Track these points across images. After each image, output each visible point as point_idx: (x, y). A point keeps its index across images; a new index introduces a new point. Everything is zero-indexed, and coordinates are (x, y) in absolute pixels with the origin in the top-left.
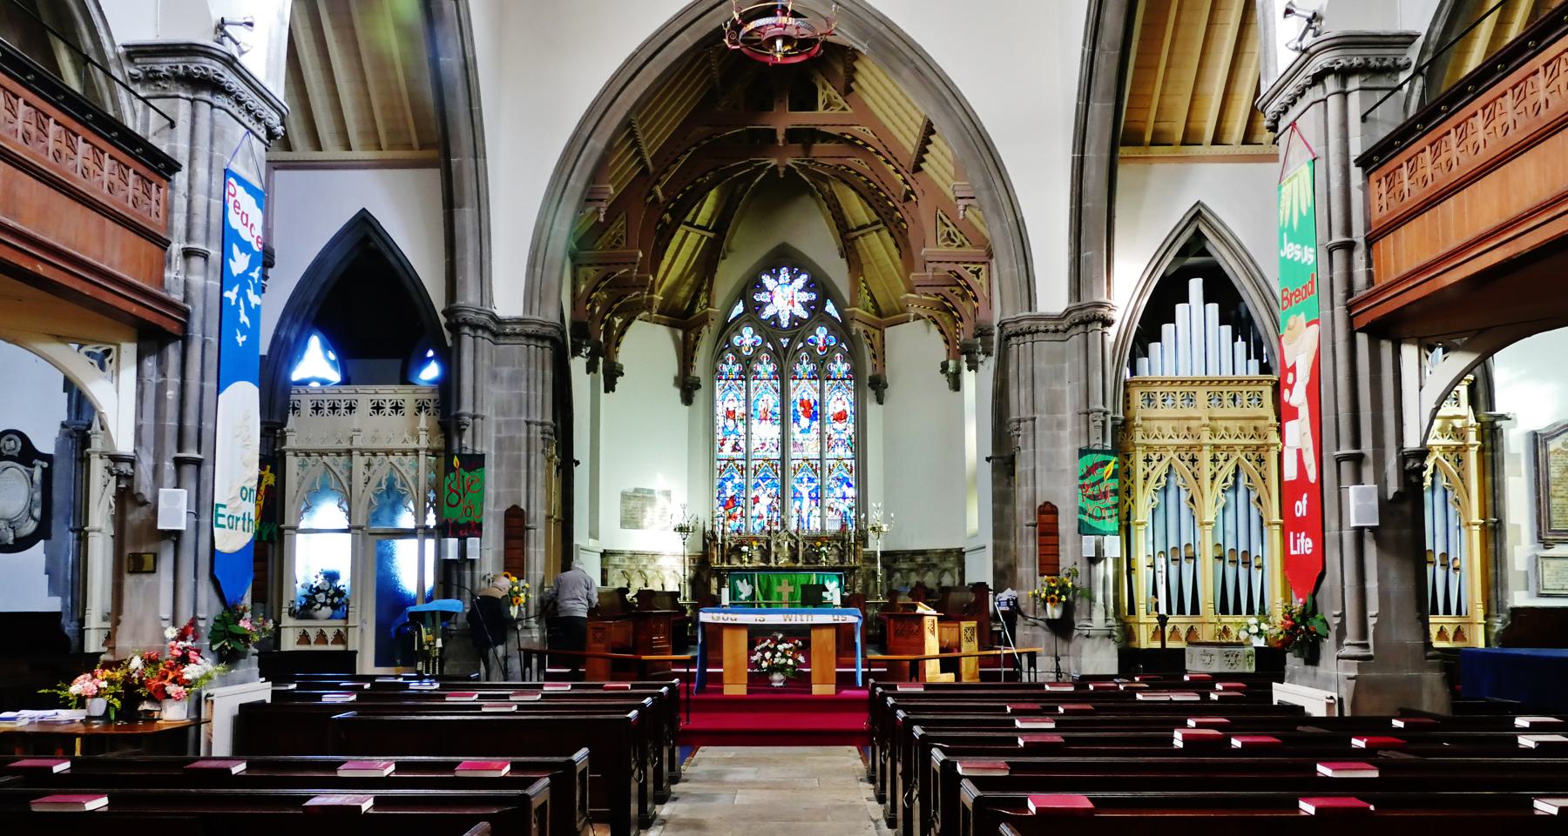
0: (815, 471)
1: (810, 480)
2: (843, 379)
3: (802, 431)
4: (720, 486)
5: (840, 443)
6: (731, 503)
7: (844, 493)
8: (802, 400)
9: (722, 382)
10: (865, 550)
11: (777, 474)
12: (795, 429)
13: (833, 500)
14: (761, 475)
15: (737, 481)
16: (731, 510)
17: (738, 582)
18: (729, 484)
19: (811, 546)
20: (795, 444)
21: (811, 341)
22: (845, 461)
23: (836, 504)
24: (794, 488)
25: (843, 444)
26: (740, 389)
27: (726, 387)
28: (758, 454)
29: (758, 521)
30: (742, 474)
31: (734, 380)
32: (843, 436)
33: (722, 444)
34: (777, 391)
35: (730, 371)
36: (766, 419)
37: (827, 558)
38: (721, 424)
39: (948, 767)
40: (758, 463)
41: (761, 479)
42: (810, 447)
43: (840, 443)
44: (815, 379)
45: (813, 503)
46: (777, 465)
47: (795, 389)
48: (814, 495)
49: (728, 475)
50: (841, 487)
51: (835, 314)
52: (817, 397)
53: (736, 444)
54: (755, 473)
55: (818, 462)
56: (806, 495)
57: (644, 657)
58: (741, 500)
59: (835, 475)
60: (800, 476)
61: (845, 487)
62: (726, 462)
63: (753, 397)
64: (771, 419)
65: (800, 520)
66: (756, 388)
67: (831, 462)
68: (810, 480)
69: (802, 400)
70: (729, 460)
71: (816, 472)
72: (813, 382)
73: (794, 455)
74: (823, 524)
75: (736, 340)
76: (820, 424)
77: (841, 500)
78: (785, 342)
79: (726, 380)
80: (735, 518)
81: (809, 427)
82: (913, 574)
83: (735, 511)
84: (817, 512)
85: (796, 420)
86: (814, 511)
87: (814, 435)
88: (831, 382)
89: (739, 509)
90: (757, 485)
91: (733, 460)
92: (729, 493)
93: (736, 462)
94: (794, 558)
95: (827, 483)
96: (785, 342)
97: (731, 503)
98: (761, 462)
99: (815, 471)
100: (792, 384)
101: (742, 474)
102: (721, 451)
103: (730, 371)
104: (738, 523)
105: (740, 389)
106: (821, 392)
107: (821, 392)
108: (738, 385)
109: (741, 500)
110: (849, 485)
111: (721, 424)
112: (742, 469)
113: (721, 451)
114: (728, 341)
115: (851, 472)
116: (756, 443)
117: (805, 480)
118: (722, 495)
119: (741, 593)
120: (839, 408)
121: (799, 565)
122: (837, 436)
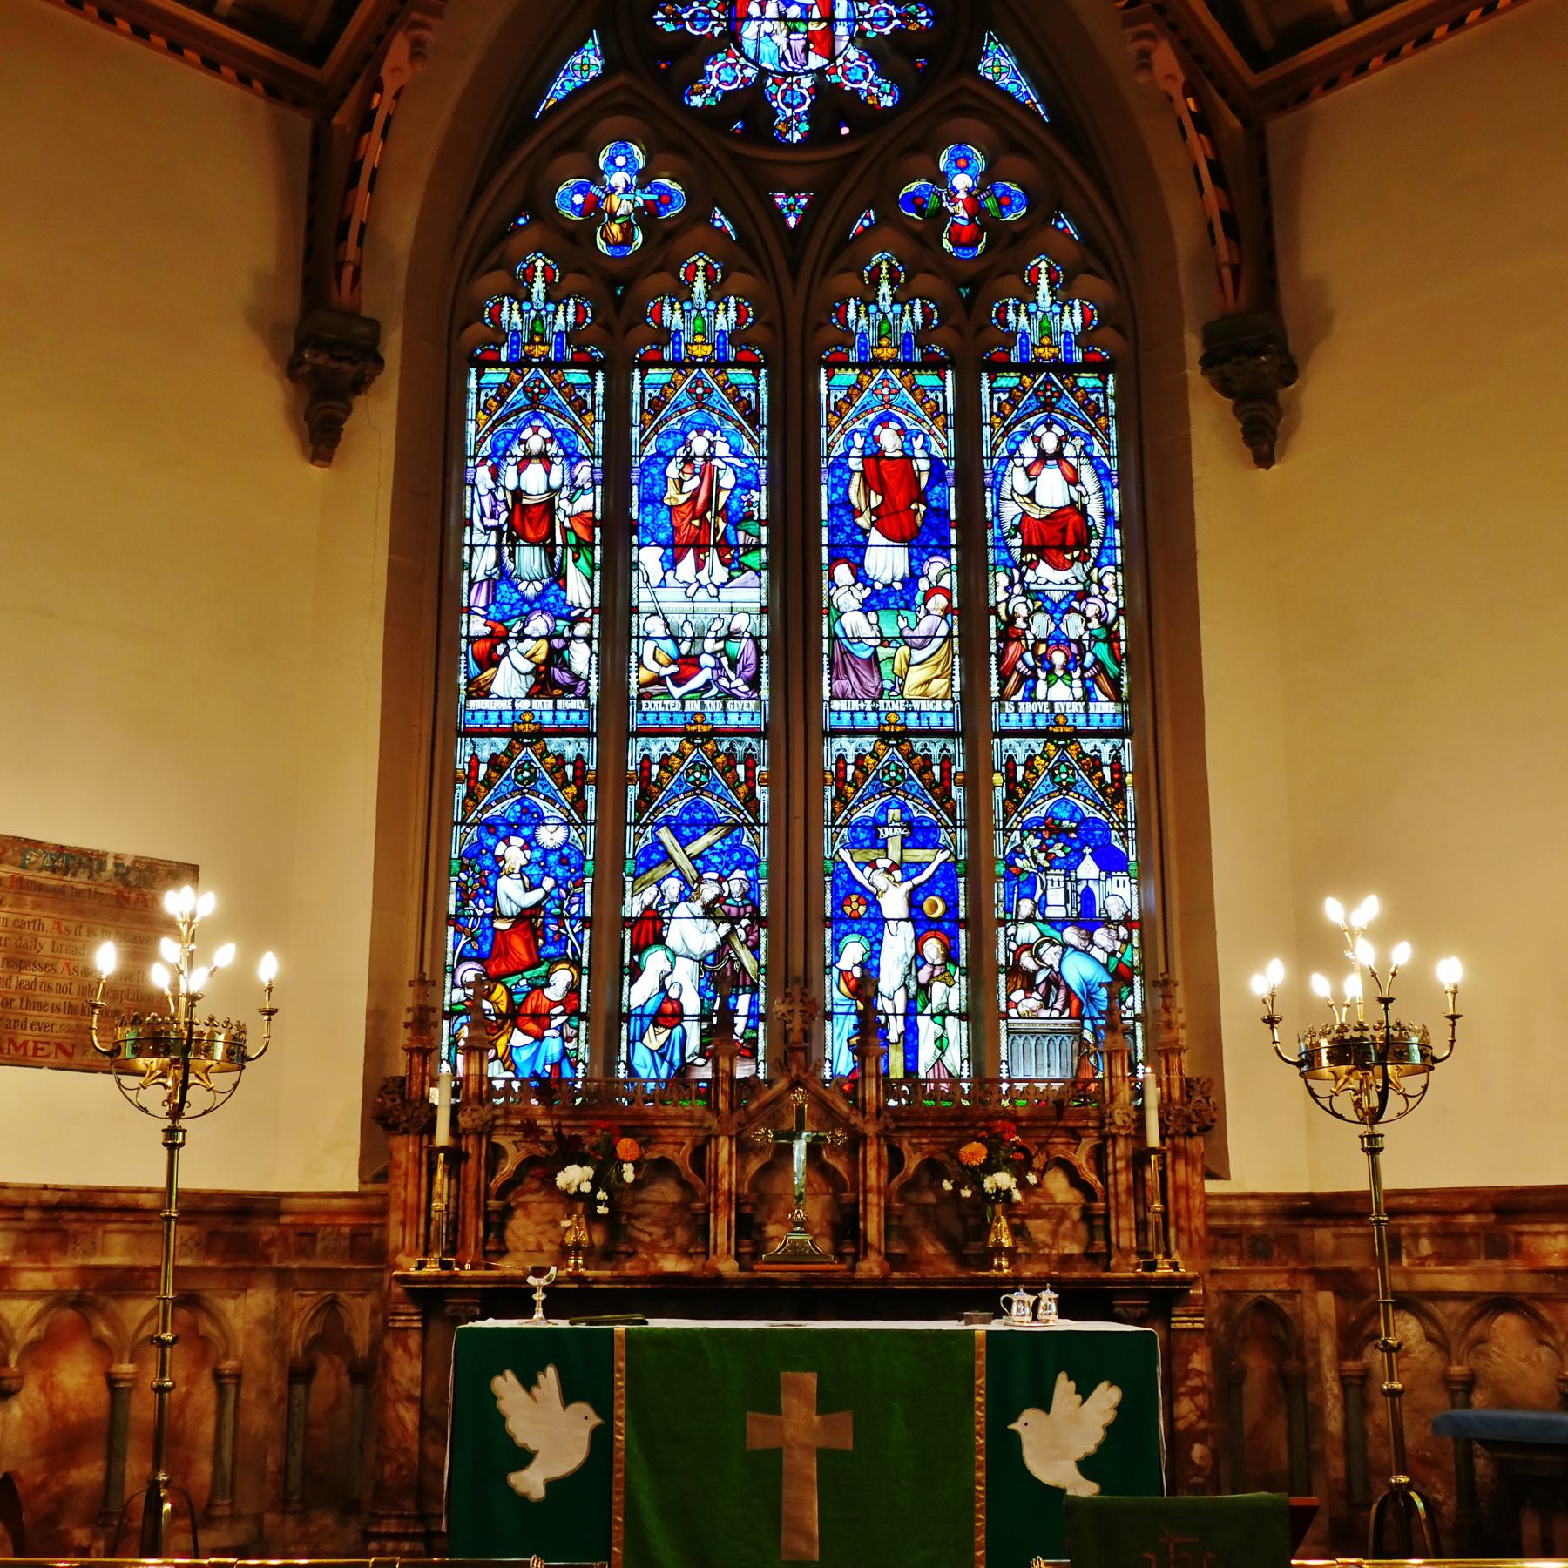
0: (941, 791)
1: (919, 835)
2: (1065, 368)
3: (874, 603)
4: (475, 853)
5: (1058, 658)
6: (519, 947)
7: (1088, 895)
8: (874, 457)
9: (495, 376)
10: (1212, 1186)
11: (751, 803)
12: (844, 592)
13: (1028, 933)
14: (675, 810)
15: (550, 836)
16: (521, 982)
17: (506, 1386)
18: (514, 854)
19: (932, 1170)
20: (842, 662)
21: (914, 201)
22: (1088, 745)
23: (1050, 955)
24: (840, 868)
25: (1073, 661)
26: (581, 407)
27: (516, 397)
28: (659, 709)
29: (655, 1038)
30: (579, 803)
31: (546, 364)
32: (1073, 626)
33: (490, 661)
34: (753, 418)
35: (536, 334)
36: (700, 547)
37: (1018, 1231)
38: (483, 562)
39: (899, 1101)
40: (656, 748)
41: (675, 827)
42: (915, 676)
43: (1058, 658)
44: (932, 364)
45: (933, 949)
46: (750, 761)
47: (838, 411)
48: (935, 907)
49: (507, 808)
50: (1070, 865)
51: (1021, 88)
52: (943, 445)
53: (556, 657)
54: (645, 799)
55: (954, 747)
56: (894, 902)
57: (575, 1286)
58: (572, 928)
59: (1040, 812)
60: (868, 811)
61: (1088, 869)
62: (501, 744)
63: (643, 445)
64: (723, 546)
65: (869, 1028)
66: (657, 405)
67: (1020, 749)
68: (919, 835)
69: (874, 457)
70: (512, 734)
71: (944, 797)
72: (927, 380)
73: (839, 712)
74: (981, 1051)
75: (569, 198)
76: (962, 570)
77: (1071, 935)
78: (791, 208)
79: (516, 365)
80: (542, 1019)
81: (910, 581)
82: (1508, 1326)
83: (538, 987)
84: (950, 994)
85: (852, 552)
86: (938, 989)
87: (932, 620)
88: (1009, 380)
89: (562, 978)
90: (655, 856)
91: (542, 733)
92: (513, 894)
93: (554, 744)
94: (845, 1227)
95: (999, 847)
96: (791, 208)
97: (519, 947)
98: (673, 744)
99: (941, 791)
100: (830, 386)
101: (579, 803)
102: (481, 690)
103: (536, 334)
104: (552, 1047)
105: (581, 407)
106: (967, 420)
107: (967, 420)
108: (569, 390)
109: (572, 928)
110: (1111, 862)
111: (483, 562)
112: (580, 779)
113: (481, 690)
114: (539, 205)
115: (1119, 796)
116: (652, 658)
117: (893, 835)
118: (484, 908)
119: (524, 1458)
120: (1053, 491)
121: (871, 1267)
122: (1041, 625)
